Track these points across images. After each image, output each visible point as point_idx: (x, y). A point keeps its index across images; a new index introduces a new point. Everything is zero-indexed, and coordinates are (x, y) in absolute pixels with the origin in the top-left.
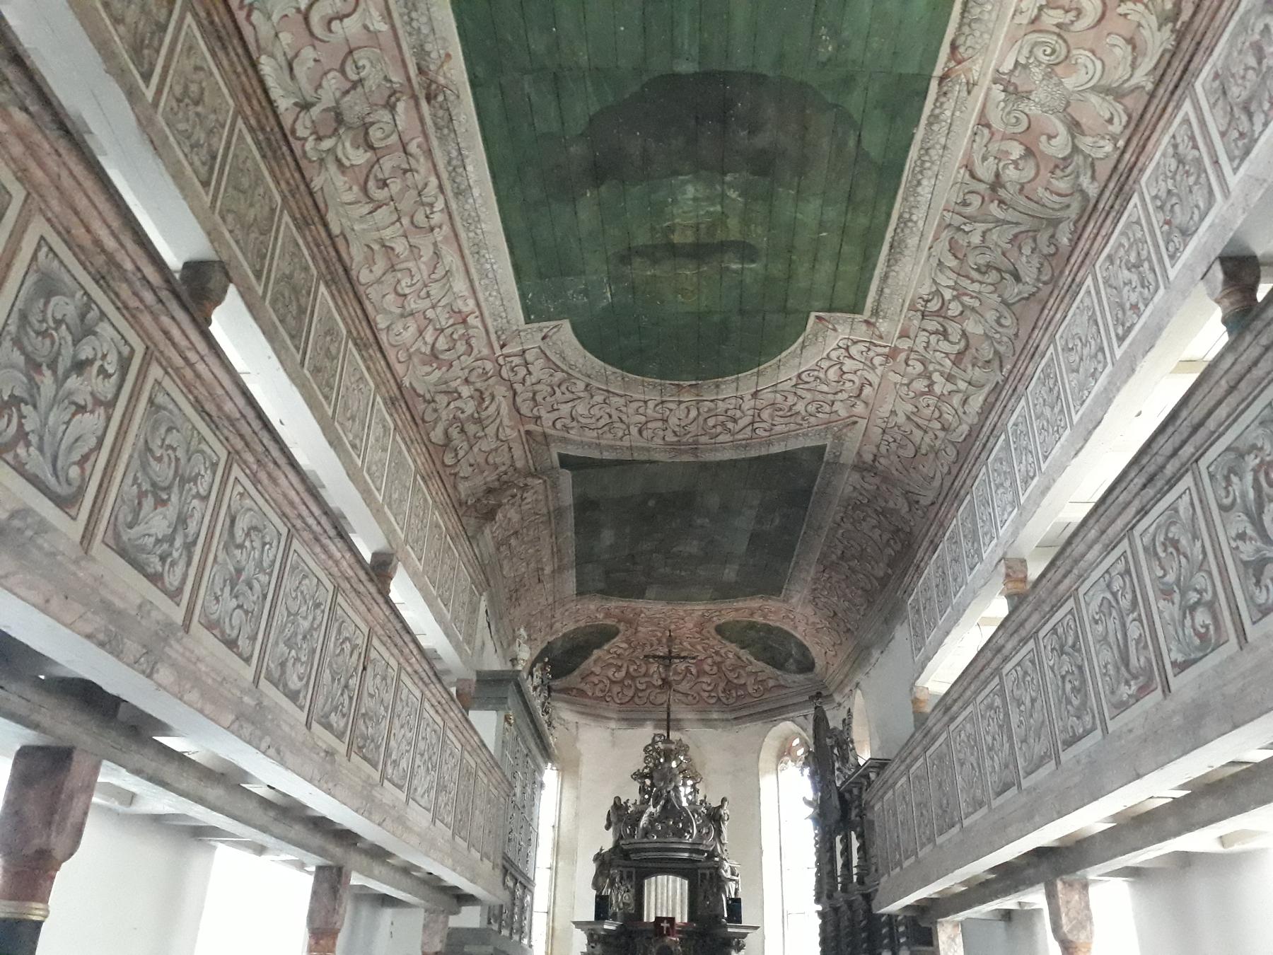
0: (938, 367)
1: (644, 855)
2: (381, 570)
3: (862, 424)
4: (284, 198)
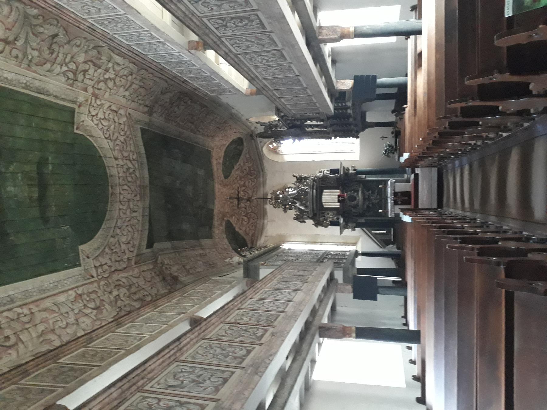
0: (102, 75)
1: (315, 208)
2: (196, 322)
3: (129, 111)
4: (13, 384)
